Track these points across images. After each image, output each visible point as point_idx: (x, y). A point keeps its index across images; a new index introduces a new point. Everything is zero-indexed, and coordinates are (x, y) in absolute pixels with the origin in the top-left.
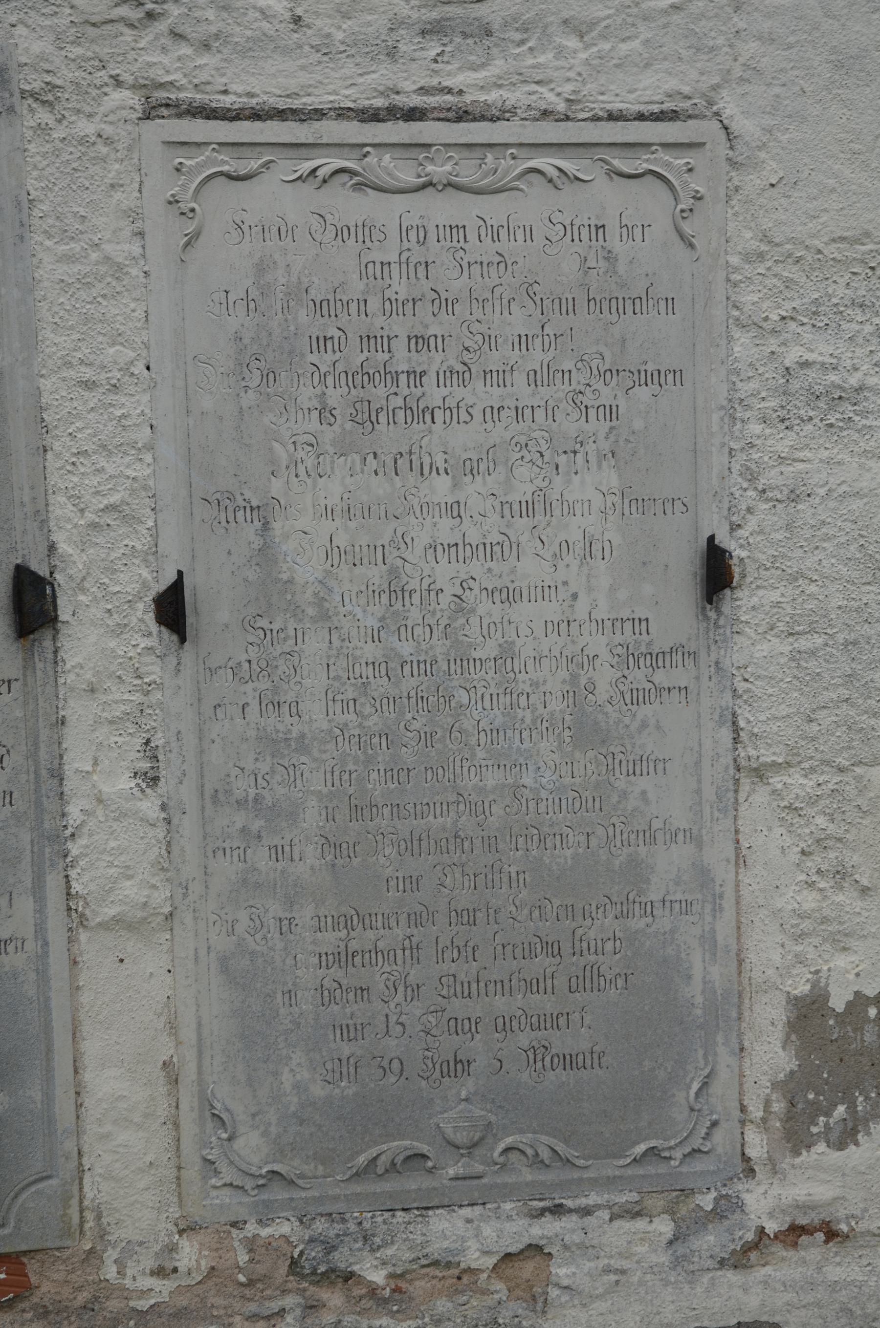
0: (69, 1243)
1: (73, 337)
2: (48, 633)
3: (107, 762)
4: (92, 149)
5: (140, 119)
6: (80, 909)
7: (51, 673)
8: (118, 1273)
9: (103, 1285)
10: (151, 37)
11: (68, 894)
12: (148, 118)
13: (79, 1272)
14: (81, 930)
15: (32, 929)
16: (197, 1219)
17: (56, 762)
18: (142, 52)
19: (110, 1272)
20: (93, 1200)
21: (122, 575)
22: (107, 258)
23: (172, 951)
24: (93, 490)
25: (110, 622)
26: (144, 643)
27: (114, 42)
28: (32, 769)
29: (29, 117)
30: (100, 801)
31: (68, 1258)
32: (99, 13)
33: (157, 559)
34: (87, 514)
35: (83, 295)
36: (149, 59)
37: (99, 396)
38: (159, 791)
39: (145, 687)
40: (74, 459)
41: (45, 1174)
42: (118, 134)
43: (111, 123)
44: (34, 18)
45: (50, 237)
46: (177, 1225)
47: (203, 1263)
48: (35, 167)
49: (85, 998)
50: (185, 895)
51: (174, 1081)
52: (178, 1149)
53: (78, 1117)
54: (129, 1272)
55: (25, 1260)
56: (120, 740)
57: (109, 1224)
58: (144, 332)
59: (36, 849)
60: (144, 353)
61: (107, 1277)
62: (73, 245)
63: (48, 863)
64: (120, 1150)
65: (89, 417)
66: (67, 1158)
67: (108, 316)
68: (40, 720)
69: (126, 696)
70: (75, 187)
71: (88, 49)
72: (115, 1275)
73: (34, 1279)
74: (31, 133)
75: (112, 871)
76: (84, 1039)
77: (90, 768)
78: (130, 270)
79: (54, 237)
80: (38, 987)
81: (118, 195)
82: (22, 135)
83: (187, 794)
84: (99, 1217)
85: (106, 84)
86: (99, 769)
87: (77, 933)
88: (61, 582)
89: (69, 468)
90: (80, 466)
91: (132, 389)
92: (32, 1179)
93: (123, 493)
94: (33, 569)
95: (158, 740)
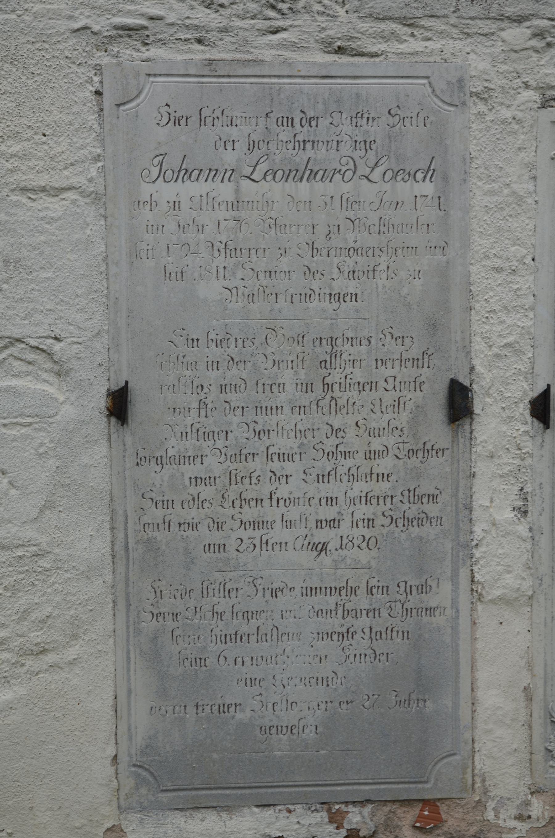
0: (465, 795)
1: (491, 241)
2: (467, 421)
3: (498, 501)
4: (509, 126)
5: (539, 108)
6: (479, 591)
7: (468, 445)
8: (495, 816)
9: (486, 823)
10: (548, 58)
11: (472, 581)
12: (544, 107)
13: (471, 814)
14: (478, 603)
15: (450, 602)
16: (541, 786)
17: (469, 500)
18: (542, 67)
19: (490, 815)
20: (480, 770)
21: (512, 386)
22: (514, 193)
23: (531, 619)
24: (498, 334)
25: (503, 415)
26: (523, 428)
27: (527, 61)
28: (454, 504)
29: (473, 108)
30: (494, 524)
31: (465, 805)
32: (519, 44)
33: (533, 377)
34: (493, 348)
35: (498, 215)
36: (547, 71)
37: (504, 276)
38: (528, 519)
39: (523, 455)
40: (487, 315)
41: (452, 752)
42: (525, 117)
43: (522, 111)
44: (480, 49)
45: (480, 179)
46: (530, 789)
47: (546, 813)
48: (475, 138)
49: (479, 645)
50: (540, 584)
51: (529, 699)
52: (531, 742)
53: (473, 719)
54: (502, 816)
55: (438, 804)
56: (506, 487)
57: (490, 786)
58: (533, 238)
59: (454, 553)
60: (532, 251)
61: (489, 818)
62: (494, 185)
63: (461, 561)
64: (497, 740)
65: (497, 289)
66: (466, 743)
67: (512, 228)
68: (460, 474)
69: (511, 461)
70: (497, 150)
71: (510, 66)
72: (493, 817)
73: (444, 816)
74: (474, 117)
75: (499, 568)
76: (478, 671)
77: (488, 504)
78: (527, 200)
79: (482, 180)
80: (452, 637)
81: (522, 154)
82: (469, 119)
83: (544, 522)
84: (484, 781)
85: (520, 87)
86: (493, 504)
87: (477, 605)
88: (476, 390)
89: (484, 320)
90: (490, 319)
91: (524, 273)
92: (444, 755)
93: (515, 336)
94: (460, 381)
95: (528, 488)
